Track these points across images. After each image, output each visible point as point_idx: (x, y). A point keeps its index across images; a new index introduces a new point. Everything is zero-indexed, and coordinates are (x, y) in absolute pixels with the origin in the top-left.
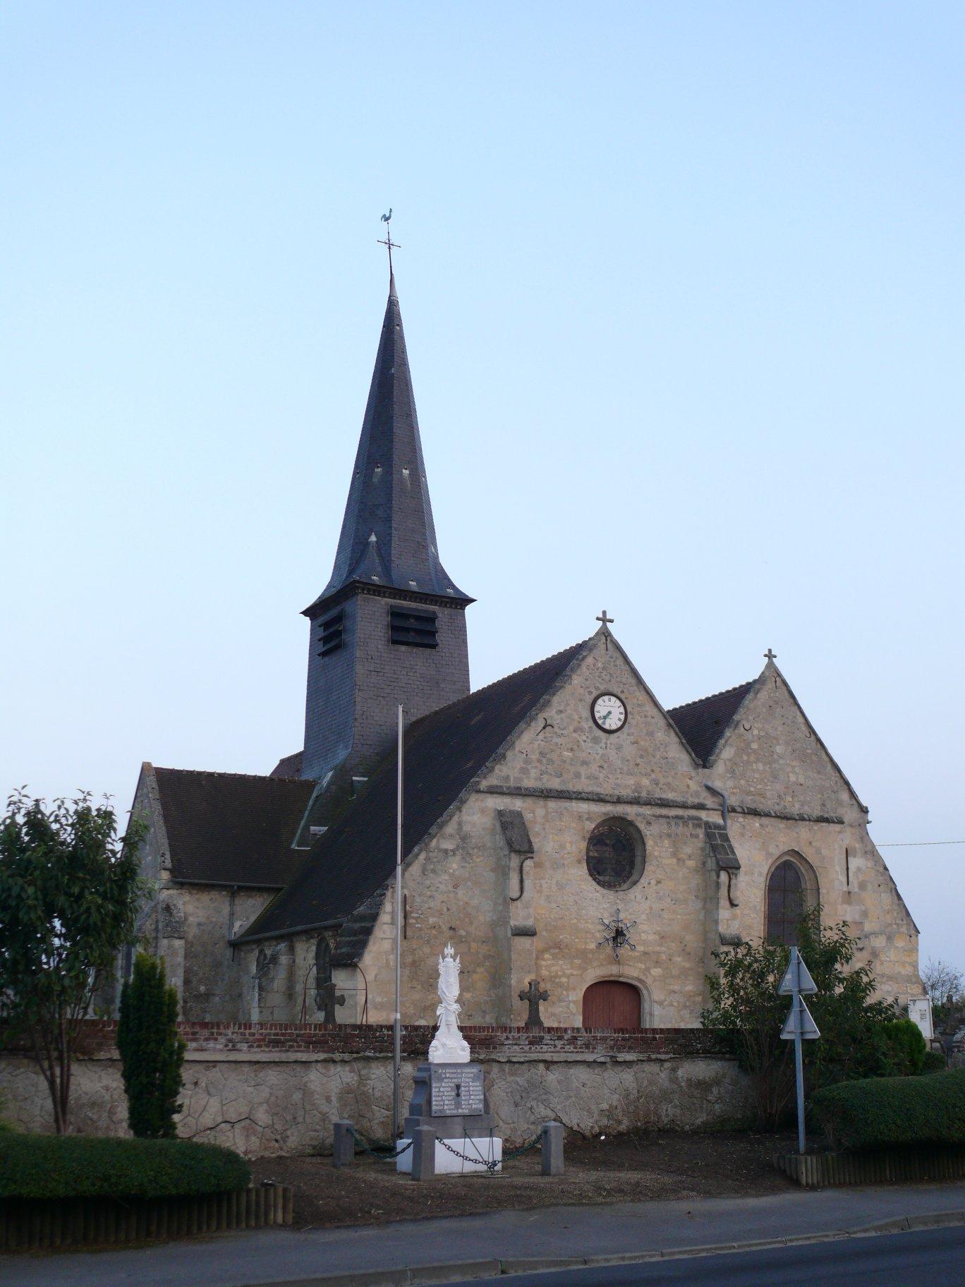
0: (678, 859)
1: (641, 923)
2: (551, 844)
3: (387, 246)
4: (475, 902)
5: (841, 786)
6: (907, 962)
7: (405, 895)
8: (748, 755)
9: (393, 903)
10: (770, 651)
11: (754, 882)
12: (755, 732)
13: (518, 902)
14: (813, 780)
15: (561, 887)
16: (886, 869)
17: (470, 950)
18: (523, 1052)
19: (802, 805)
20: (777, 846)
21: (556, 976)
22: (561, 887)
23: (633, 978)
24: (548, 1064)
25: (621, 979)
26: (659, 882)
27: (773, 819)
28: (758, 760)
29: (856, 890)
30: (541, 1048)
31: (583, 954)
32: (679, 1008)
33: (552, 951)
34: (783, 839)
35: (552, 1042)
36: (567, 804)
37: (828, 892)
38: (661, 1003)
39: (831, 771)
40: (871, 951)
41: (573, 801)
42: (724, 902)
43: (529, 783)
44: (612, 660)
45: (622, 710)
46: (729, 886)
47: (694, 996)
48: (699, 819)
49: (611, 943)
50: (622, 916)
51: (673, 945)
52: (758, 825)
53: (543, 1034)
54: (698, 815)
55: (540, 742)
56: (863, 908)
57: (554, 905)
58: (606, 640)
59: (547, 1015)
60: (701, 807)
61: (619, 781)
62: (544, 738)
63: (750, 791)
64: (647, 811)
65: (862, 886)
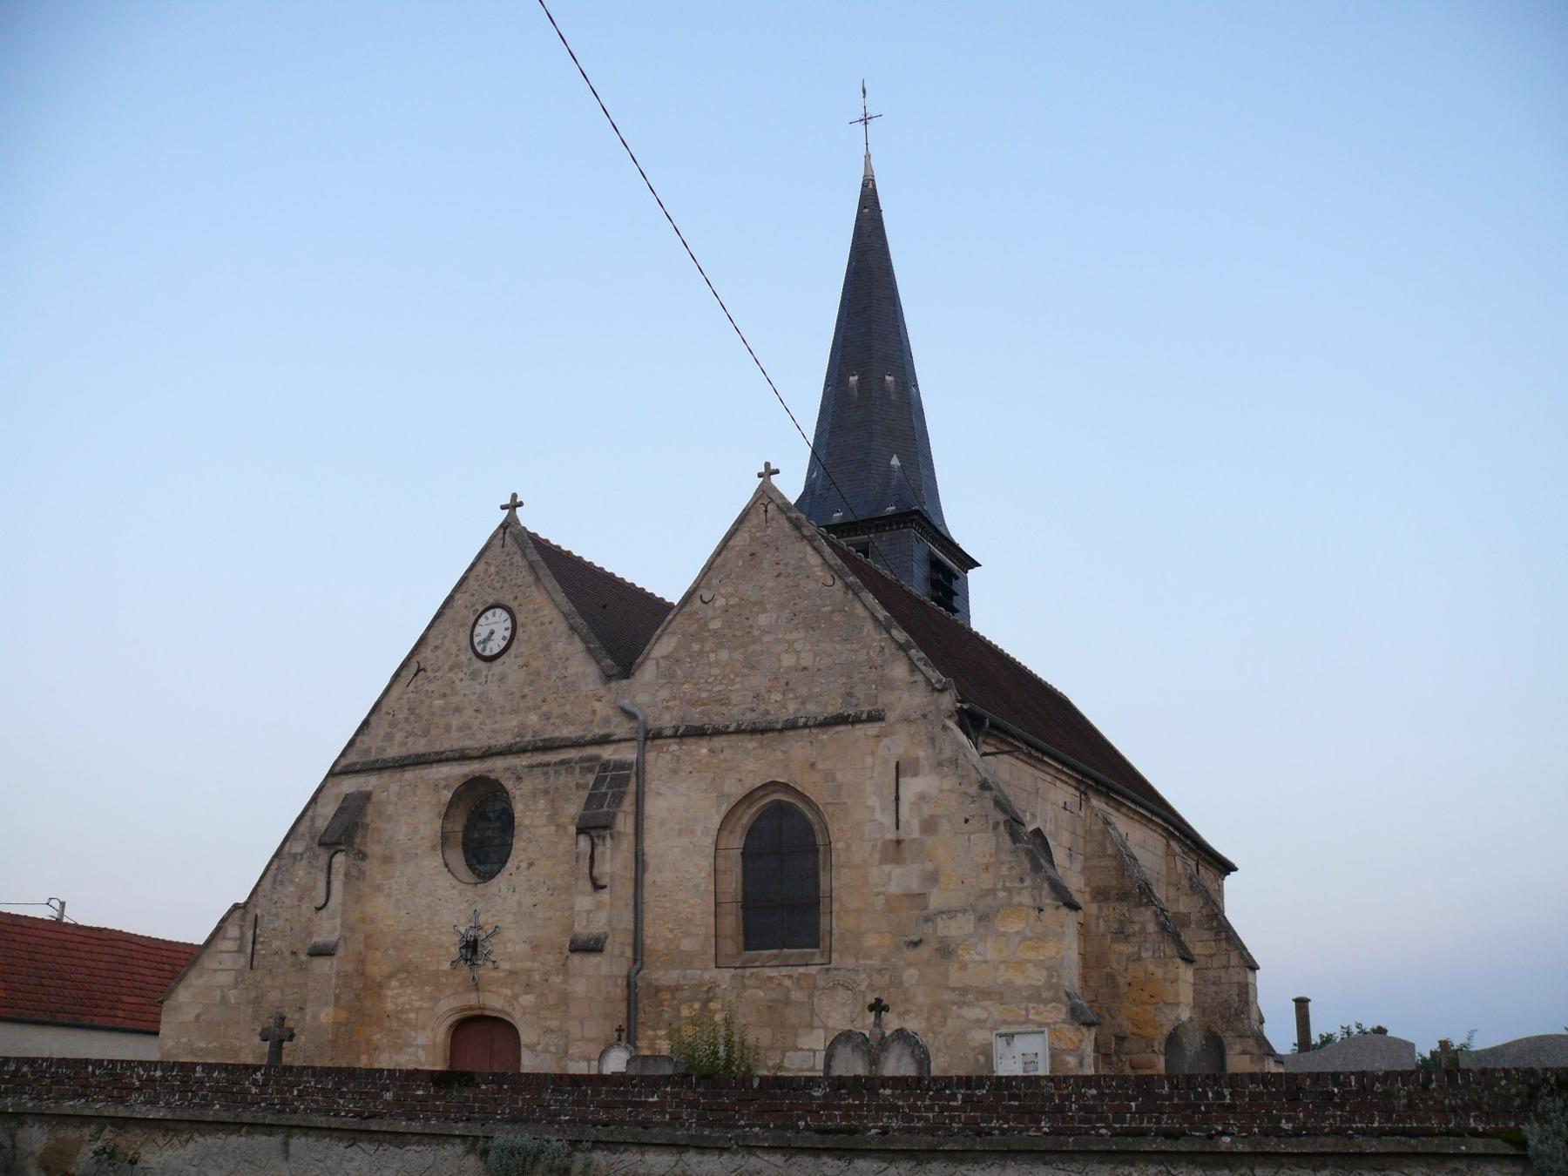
0: (558, 826)
1: (507, 928)
6: (1029, 961)
7: (257, 915)
9: (242, 927)
12: (720, 602)
19: (803, 703)
21: (403, 1011)
23: (499, 1011)
25: (488, 1013)
26: (531, 864)
27: (735, 738)
28: (720, 646)
29: (916, 835)
33: (400, 976)
37: (848, 847)
38: (532, 1048)
39: (872, 631)
43: (393, 752)
48: (597, 758)
50: (482, 920)
52: (704, 751)
56: (929, 866)
60: (604, 740)
61: (497, 726)
63: (700, 699)
64: (522, 761)
65: (929, 826)
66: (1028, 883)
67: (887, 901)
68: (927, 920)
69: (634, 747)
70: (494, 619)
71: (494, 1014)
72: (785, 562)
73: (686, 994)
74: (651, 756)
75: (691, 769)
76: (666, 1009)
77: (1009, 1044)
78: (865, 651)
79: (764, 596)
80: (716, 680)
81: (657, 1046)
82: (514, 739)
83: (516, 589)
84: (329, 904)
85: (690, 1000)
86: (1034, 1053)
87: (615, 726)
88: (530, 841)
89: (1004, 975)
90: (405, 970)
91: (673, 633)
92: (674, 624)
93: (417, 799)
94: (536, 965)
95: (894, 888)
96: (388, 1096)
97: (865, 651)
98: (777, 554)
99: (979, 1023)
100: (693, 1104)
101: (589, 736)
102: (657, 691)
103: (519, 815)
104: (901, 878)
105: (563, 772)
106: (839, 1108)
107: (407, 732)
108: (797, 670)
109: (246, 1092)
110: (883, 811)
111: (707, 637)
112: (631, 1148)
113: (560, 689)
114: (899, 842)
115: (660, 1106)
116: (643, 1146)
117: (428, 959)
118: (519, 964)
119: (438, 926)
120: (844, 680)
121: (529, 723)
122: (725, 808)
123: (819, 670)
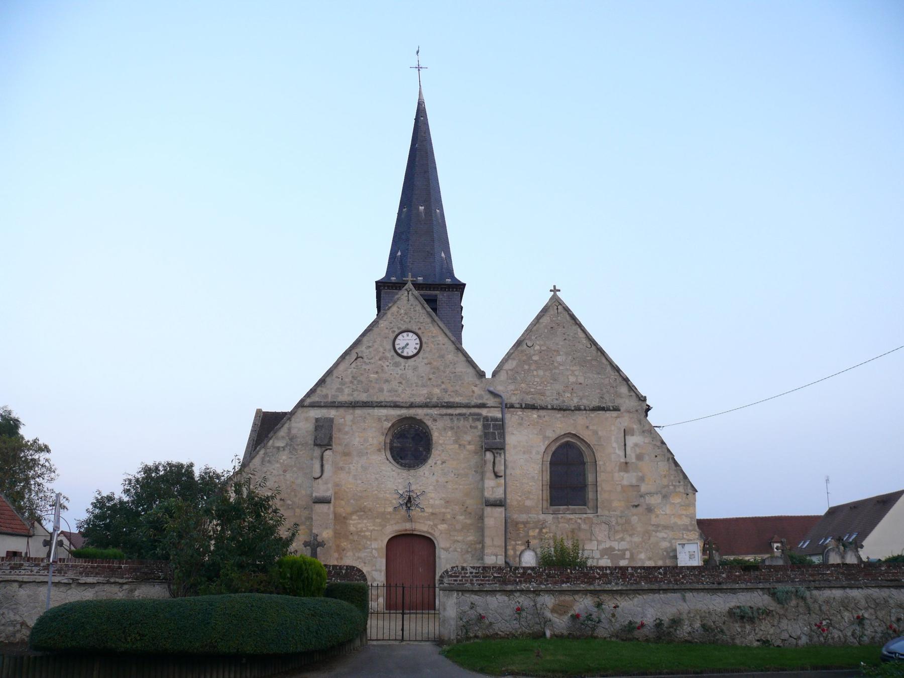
2: (358, 439)
3: (417, 69)
4: (299, 481)
5: (620, 382)
6: (683, 515)
8: (529, 365)
10: (555, 287)
11: (532, 459)
12: (537, 348)
13: (320, 479)
14: (592, 379)
15: (365, 469)
16: (663, 443)
17: (294, 514)
18: (4, 575)
19: (581, 399)
20: (554, 431)
22: (365, 469)
23: (424, 532)
24: (21, 583)
25: (415, 533)
26: (443, 462)
28: (538, 368)
30: (20, 572)
31: (383, 515)
32: (462, 553)
33: (358, 514)
34: (560, 425)
35: (30, 568)
36: (370, 411)
37: (605, 464)
38: (446, 550)
39: (610, 371)
40: (646, 507)
41: (376, 408)
42: (489, 475)
43: (343, 398)
44: (412, 307)
45: (418, 341)
46: (494, 463)
47: (475, 544)
48: (480, 415)
49: (404, 507)
50: (413, 487)
51: (457, 507)
52: (535, 416)
53: (22, 563)
54: (481, 411)
55: (352, 369)
56: (640, 474)
57: (359, 482)
58: (408, 294)
59: (355, 558)
60: (483, 406)
61: (414, 392)
62: (356, 366)
63: (530, 392)
64: (435, 411)
65: (640, 457)
66: (682, 483)
67: (622, 487)
68: (641, 496)
69: (498, 411)
70: (408, 338)
71: (419, 533)
72: (568, 334)
73: (531, 525)
74: (508, 416)
75: (528, 424)
76: (521, 532)
77: (683, 548)
78: (608, 379)
79: (558, 348)
80: (537, 384)
81: (517, 549)
82: (426, 400)
83: (419, 324)
84: (323, 477)
85: (534, 528)
86: (694, 550)
87: (487, 400)
88: (443, 451)
89: (673, 520)
90: (362, 511)
91: (514, 359)
92: (513, 355)
93: (366, 424)
94: (448, 510)
95: (625, 482)
96: (724, 575)
97: (608, 379)
98: (564, 329)
99: (664, 539)
100: (843, 573)
101: (473, 403)
102: (507, 385)
103: (436, 438)
104: (628, 478)
105: (462, 419)
106: (890, 573)
107: (353, 389)
108: (577, 384)
109: (656, 577)
110: (619, 449)
111: (532, 363)
112: (826, 589)
113: (452, 378)
114: (626, 463)
115: (831, 574)
116: (830, 588)
117: (378, 506)
118: (437, 510)
119: (384, 490)
120: (598, 391)
121: (435, 392)
122: (547, 443)
123: (587, 385)
